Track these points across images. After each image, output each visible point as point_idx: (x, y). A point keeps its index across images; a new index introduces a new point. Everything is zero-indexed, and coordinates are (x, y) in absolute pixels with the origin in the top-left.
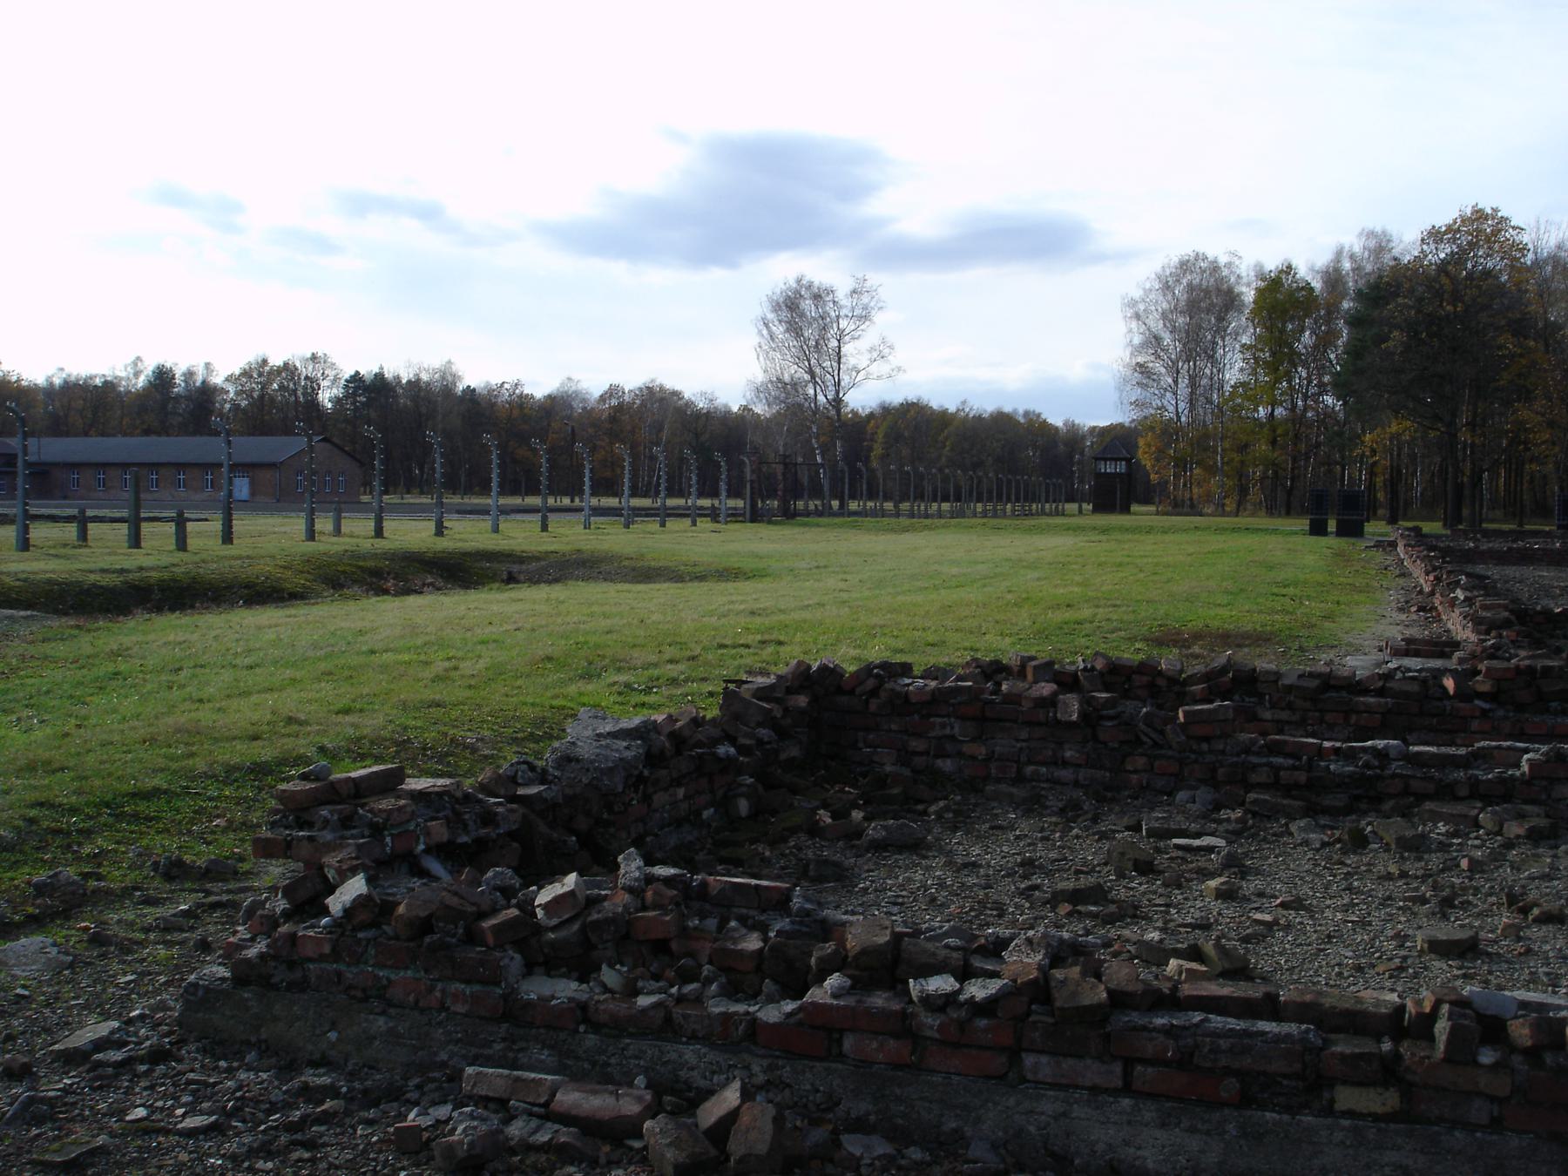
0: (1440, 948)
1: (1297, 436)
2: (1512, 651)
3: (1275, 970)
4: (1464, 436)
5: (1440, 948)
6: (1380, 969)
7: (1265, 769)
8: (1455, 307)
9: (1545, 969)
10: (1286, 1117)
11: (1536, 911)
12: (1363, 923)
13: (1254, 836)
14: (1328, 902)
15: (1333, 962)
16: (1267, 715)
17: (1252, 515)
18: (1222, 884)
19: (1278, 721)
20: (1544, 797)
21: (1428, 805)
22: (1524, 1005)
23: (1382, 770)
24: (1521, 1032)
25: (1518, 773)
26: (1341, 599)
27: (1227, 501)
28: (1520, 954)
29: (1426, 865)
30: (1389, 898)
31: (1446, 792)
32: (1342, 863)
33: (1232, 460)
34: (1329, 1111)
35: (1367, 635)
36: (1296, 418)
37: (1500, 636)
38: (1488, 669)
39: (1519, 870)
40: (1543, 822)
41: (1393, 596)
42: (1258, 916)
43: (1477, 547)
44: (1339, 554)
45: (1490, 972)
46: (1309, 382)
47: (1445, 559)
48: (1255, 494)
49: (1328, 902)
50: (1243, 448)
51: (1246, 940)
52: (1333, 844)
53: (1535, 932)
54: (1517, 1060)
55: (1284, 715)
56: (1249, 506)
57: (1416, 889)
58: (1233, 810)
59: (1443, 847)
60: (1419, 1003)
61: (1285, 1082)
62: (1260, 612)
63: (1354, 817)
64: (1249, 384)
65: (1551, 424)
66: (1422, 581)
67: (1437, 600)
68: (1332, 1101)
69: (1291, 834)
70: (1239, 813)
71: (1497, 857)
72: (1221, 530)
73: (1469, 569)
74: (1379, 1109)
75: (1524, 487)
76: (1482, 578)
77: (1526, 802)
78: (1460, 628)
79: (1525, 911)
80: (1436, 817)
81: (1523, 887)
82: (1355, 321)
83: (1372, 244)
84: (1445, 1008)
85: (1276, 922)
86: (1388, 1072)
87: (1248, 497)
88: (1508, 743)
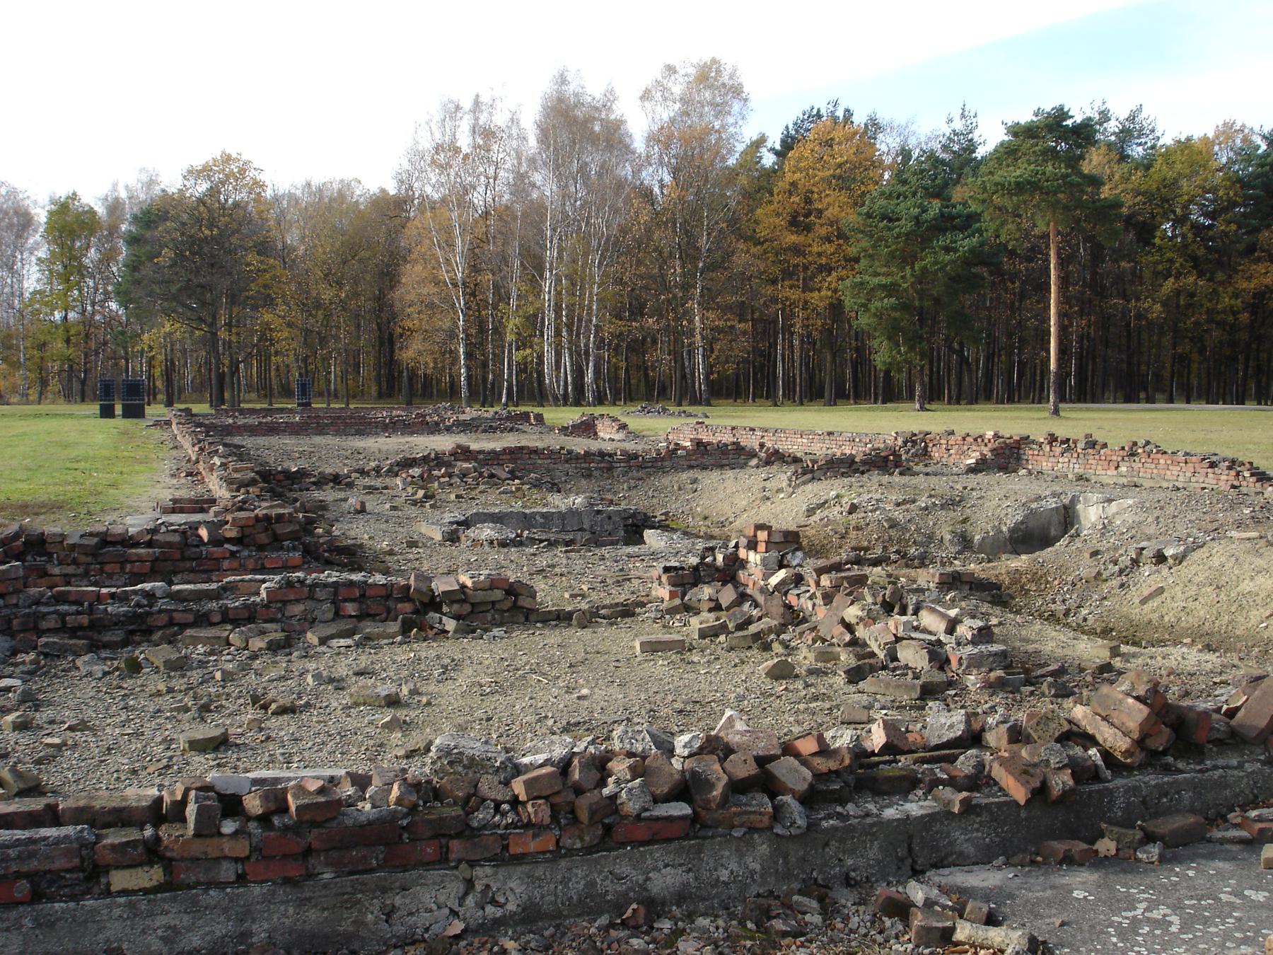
0: (199, 746)
1: (87, 336)
2: (256, 504)
3: (64, 784)
4: (223, 334)
5: (199, 746)
6: (150, 770)
7: (54, 616)
8: (212, 231)
9: (282, 751)
10: (72, 905)
11: (273, 706)
12: (138, 734)
13: (45, 674)
14: (109, 721)
15: (113, 770)
16: (56, 571)
17: (53, 403)
18: (18, 717)
19: (66, 575)
20: (279, 616)
21: (189, 632)
22: (255, 782)
23: (151, 608)
24: (254, 804)
25: (258, 600)
26: (124, 470)
27: (31, 391)
28: (262, 742)
29: (189, 680)
30: (159, 711)
31: (203, 620)
32: (120, 687)
33: (33, 357)
34: (107, 893)
35: (144, 498)
36: (87, 322)
37: (248, 492)
38: (234, 519)
39: (261, 675)
40: (279, 636)
41: (168, 466)
42: (49, 740)
43: (235, 423)
44: (125, 433)
45: (238, 760)
46: (96, 290)
47: (207, 432)
48: (54, 384)
49: (109, 721)
50: (42, 346)
51: (39, 762)
52: (113, 672)
53: (274, 722)
54: (252, 826)
55: (70, 570)
56: (50, 396)
57: (181, 701)
58: (28, 653)
59: (202, 664)
60: (172, 793)
61: (68, 876)
62: (55, 484)
63: (130, 648)
64: (45, 291)
65: (289, 325)
66: (190, 452)
67: (201, 466)
68: (109, 884)
69: (78, 668)
70: (32, 656)
71: (244, 668)
72: (24, 417)
73: (228, 440)
74: (148, 885)
75: (272, 374)
76: (237, 446)
77: (266, 621)
78: (217, 488)
79: (265, 707)
80: (195, 641)
81: (265, 688)
82: (133, 240)
83: (145, 178)
84: (193, 794)
85: (64, 744)
86: (152, 853)
87: (49, 388)
88: (250, 576)
